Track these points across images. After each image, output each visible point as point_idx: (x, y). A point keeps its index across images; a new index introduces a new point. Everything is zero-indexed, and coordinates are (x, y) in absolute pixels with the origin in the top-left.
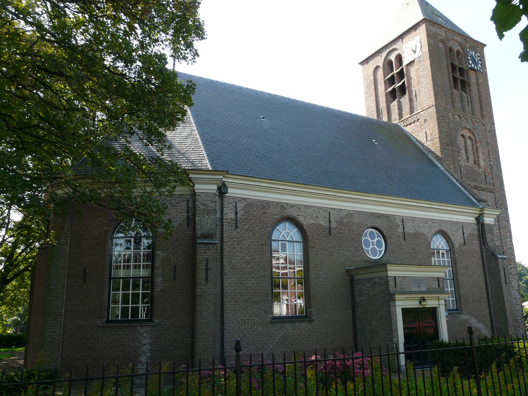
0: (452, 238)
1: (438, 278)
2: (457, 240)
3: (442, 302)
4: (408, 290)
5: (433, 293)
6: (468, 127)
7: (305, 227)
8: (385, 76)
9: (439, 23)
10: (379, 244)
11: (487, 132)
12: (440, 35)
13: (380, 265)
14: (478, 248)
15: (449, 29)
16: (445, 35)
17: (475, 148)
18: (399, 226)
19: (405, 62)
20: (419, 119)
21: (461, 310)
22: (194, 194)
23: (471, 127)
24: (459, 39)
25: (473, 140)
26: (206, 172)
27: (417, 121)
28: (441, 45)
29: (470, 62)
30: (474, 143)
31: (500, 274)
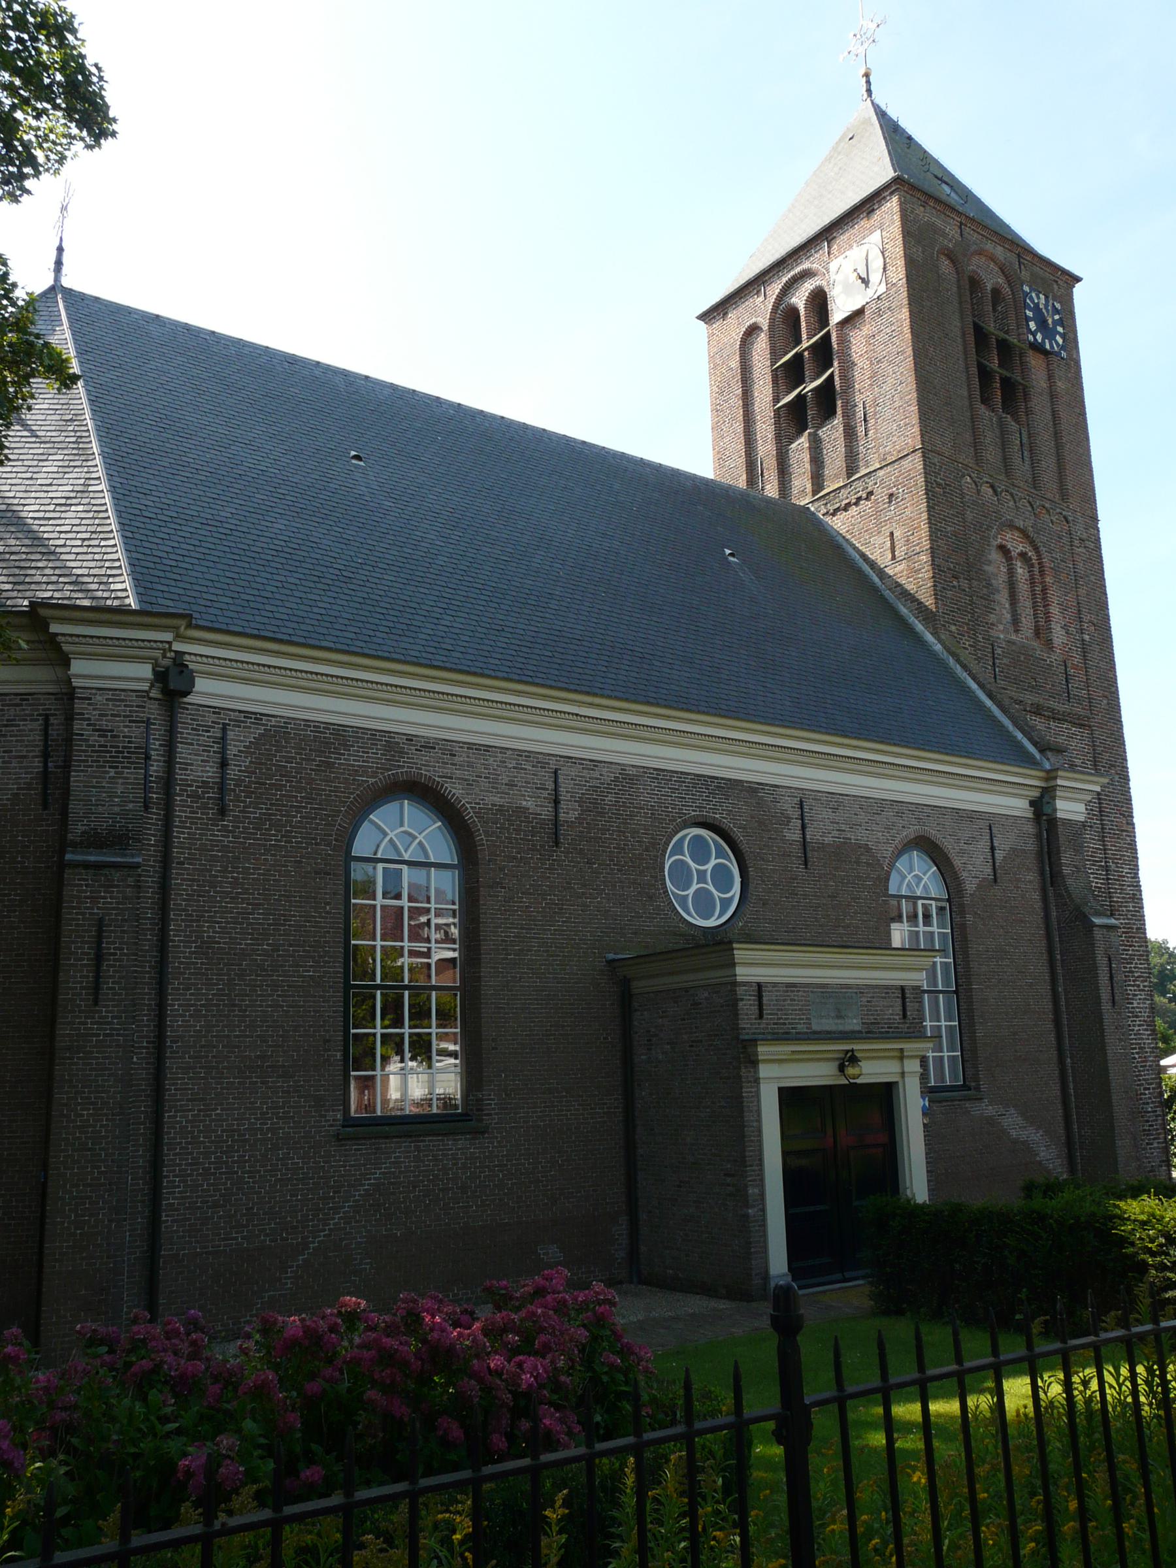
0: (957, 862)
1: (903, 988)
2: (974, 867)
3: (913, 1066)
4: (802, 1028)
5: (885, 1036)
6: (1021, 524)
7: (470, 815)
8: (775, 355)
9: (944, 198)
10: (721, 878)
11: (1076, 543)
12: (944, 235)
13: (717, 945)
14: (1036, 896)
15: (973, 220)
16: (957, 236)
17: (1038, 589)
18: (789, 819)
19: (836, 317)
20: (871, 493)
21: (978, 1089)
22: (68, 694)
23: (1029, 523)
24: (999, 252)
25: (1032, 566)
26: (118, 615)
27: (867, 499)
28: (945, 266)
29: (1032, 325)
30: (1037, 573)
31: (1096, 976)
